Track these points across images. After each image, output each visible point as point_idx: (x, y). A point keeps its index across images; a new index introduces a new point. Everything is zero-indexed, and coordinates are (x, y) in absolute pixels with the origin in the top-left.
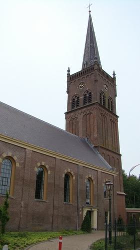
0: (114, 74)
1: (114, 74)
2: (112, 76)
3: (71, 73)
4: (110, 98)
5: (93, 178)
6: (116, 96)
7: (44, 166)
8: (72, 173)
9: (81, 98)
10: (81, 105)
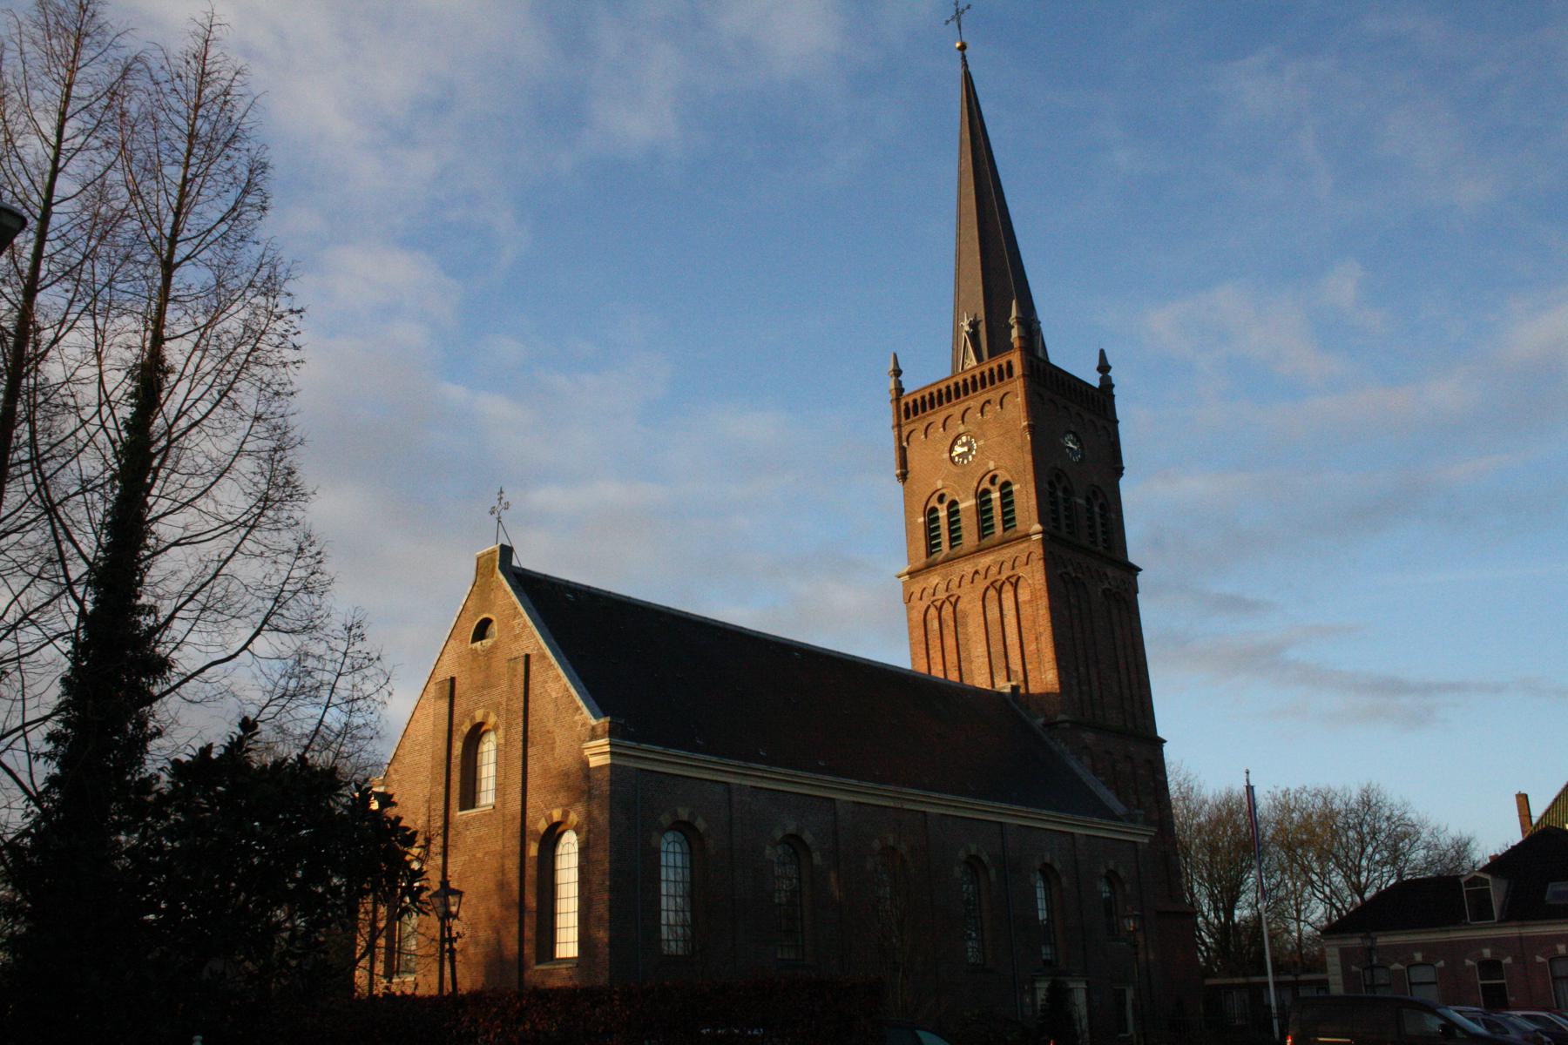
0: (1104, 368)
1: (1104, 368)
2: (1094, 380)
3: (911, 384)
5: (1057, 866)
6: (1119, 471)
9: (967, 504)
10: (970, 536)
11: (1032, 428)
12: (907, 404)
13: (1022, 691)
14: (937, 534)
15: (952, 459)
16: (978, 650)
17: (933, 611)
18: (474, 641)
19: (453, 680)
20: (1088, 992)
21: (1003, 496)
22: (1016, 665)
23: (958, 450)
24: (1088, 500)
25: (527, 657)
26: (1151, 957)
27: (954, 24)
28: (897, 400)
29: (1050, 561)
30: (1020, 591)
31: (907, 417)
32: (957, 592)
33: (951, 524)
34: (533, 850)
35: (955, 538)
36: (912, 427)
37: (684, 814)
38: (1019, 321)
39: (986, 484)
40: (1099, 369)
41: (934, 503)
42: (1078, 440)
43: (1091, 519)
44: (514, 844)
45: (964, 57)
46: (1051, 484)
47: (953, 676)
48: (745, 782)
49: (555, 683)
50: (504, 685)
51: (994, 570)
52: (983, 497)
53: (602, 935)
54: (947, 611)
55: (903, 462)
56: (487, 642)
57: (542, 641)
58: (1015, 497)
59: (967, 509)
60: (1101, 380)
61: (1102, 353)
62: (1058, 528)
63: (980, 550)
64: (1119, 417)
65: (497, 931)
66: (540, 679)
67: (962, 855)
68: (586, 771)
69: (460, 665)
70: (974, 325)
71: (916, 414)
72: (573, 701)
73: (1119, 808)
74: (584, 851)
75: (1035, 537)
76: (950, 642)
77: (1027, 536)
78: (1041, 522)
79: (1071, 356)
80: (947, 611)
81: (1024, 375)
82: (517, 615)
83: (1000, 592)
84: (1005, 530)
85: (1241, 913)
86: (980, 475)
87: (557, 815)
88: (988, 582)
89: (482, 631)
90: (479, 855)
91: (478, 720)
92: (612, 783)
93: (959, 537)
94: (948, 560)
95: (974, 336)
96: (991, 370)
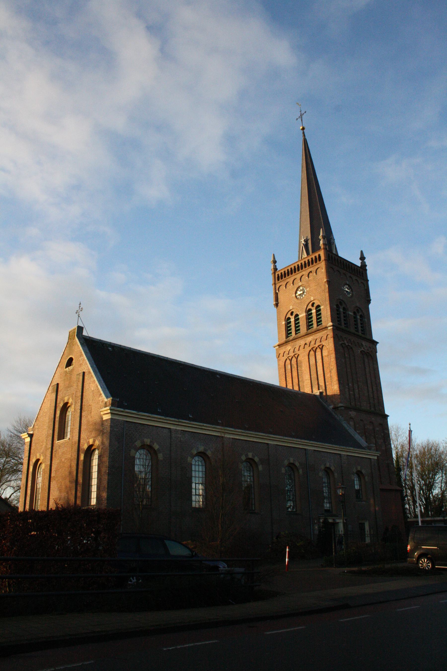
0: (362, 258)
1: (362, 258)
3: (281, 266)
4: (358, 310)
5: (333, 468)
6: (369, 301)
7: (293, 464)
8: (297, 464)
9: (302, 315)
11: (329, 282)
12: (278, 275)
13: (324, 394)
14: (291, 328)
15: (296, 297)
16: (306, 377)
17: (288, 361)
18: (66, 368)
19: (58, 384)
20: (345, 524)
21: (317, 311)
22: (322, 383)
23: (299, 293)
24: (354, 313)
25: (84, 373)
26: (377, 509)
27: (300, 120)
28: (274, 273)
29: (336, 338)
30: (323, 351)
31: (278, 280)
32: (298, 352)
33: (296, 324)
34: (82, 457)
35: (297, 330)
36: (280, 284)
37: (147, 441)
38: (324, 237)
39: (310, 306)
40: (361, 259)
41: (289, 315)
42: (350, 287)
43: (356, 321)
44: (75, 454)
45: (304, 133)
46: (337, 306)
47: (296, 388)
48: (178, 428)
49: (94, 384)
50: (75, 387)
51: (313, 343)
52: (308, 312)
53: (104, 495)
54: (294, 360)
55: (277, 299)
56: (71, 368)
57: (89, 366)
58: (322, 312)
59: (302, 317)
60: (361, 263)
61: (362, 252)
62: (340, 324)
63: (307, 335)
64: (369, 279)
65: (68, 493)
66: (88, 382)
67: (286, 462)
68: (102, 422)
69: (61, 378)
70: (306, 241)
71: (282, 278)
72: (99, 391)
73: (363, 443)
74: (100, 457)
75: (329, 328)
76: (295, 374)
77: (326, 328)
78: (332, 322)
79: (348, 252)
80: (294, 360)
81: (325, 260)
82: (81, 355)
83: (315, 352)
84: (318, 326)
85: (436, 491)
86: (307, 303)
87: (91, 442)
88: (310, 348)
89: (70, 362)
90: (63, 460)
91: (66, 401)
92: (111, 426)
93: (299, 329)
94: (294, 339)
95: (306, 246)
96: (312, 259)
